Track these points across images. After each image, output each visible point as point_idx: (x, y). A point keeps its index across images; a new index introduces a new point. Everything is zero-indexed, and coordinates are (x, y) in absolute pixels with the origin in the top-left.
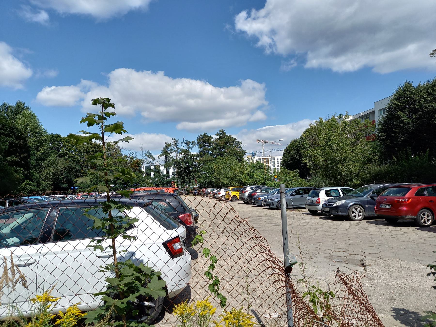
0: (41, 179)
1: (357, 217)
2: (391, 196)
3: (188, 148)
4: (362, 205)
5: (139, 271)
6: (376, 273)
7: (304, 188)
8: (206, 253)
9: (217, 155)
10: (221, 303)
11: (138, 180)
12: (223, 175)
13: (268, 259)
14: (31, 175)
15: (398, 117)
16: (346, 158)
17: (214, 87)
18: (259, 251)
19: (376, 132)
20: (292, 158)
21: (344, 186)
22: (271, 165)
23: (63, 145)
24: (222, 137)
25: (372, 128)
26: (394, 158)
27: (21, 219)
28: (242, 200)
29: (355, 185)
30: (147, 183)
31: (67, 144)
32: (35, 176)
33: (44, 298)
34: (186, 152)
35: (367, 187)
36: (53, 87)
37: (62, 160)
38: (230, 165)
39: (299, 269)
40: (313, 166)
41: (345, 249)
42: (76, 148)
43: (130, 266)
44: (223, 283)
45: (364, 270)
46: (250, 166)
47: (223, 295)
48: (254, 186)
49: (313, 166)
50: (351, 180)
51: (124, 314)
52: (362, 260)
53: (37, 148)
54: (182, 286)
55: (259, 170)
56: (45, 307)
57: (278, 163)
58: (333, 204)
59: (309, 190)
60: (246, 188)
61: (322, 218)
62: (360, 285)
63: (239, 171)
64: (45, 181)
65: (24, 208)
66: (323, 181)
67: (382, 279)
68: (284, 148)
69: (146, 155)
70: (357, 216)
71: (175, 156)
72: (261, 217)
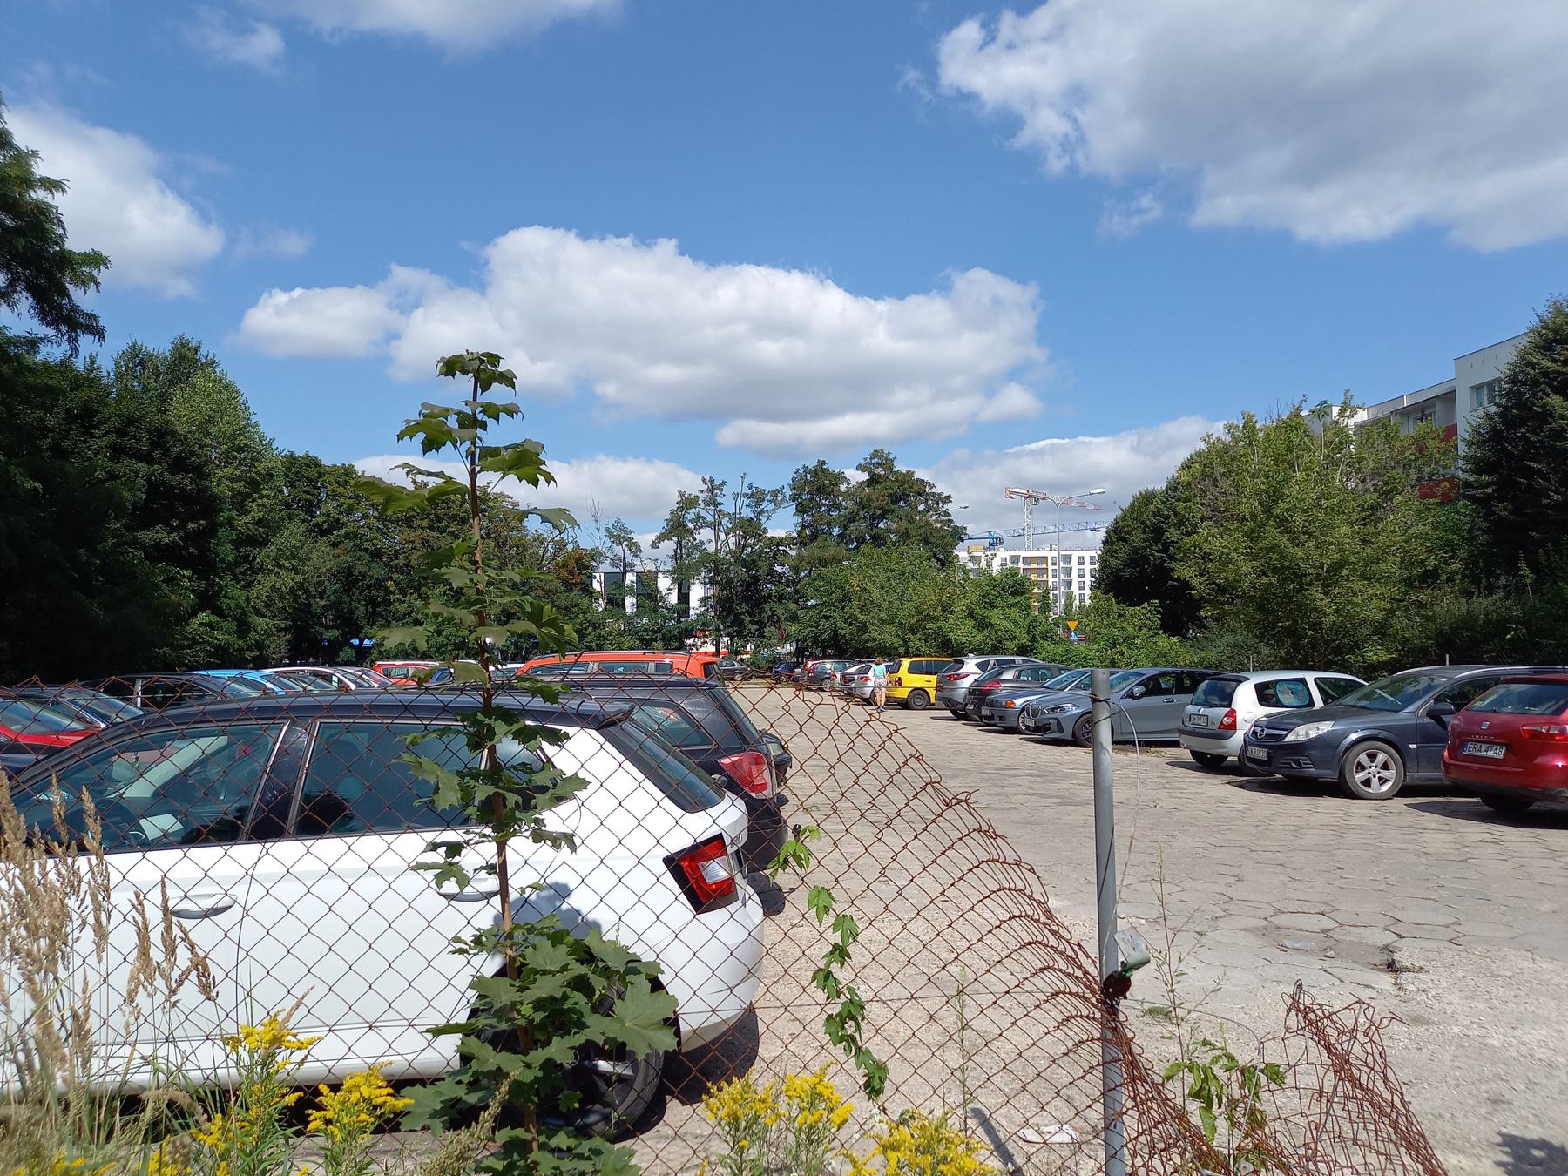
0: (253, 608)
1: (1375, 788)
2: (1507, 715)
3: (759, 515)
4: (1395, 741)
5: (586, 955)
6: (1438, 997)
7: (1178, 670)
8: (821, 905)
9: (861, 540)
10: (867, 1085)
11: (581, 624)
12: (882, 615)
13: (1051, 964)
14: (217, 594)
16: (1341, 564)
17: (852, 297)
18: (1008, 910)
19: (1460, 470)
20: (1136, 559)
21: (1325, 670)
22: (1057, 580)
23: (327, 495)
24: (879, 475)
25: (1444, 454)
26: (1525, 571)
27: (186, 754)
28: (947, 706)
29: (1371, 665)
30: (610, 633)
31: (341, 490)
32: (232, 598)
33: (268, 1037)
34: (750, 528)
35: (1415, 678)
36: (298, 292)
37: (323, 545)
38: (904, 578)
39: (1157, 974)
40: (1213, 590)
41: (1327, 904)
42: (372, 505)
43: (557, 938)
44: (874, 1011)
45: (1396, 984)
46: (977, 584)
47: (875, 1056)
48: (993, 659)
49: (1213, 590)
50: (1356, 647)
51: (533, 1102)
52: (1387, 949)
53: (240, 503)
54: (731, 1009)
55: (1013, 601)
56: (268, 1068)
57: (1081, 576)
58: (1285, 732)
59: (1196, 679)
60: (963, 663)
61: (1241, 786)
62: (1380, 1048)
63: (939, 600)
64: (264, 616)
65: (204, 717)
66: (1249, 647)
67: (1463, 1025)
68: (1106, 521)
69: (610, 535)
70: (1375, 781)
71: (710, 541)
72: (1014, 772)
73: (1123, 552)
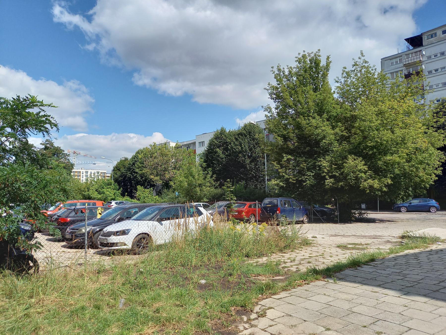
15: (216, 152)
50: (202, 199)
68: (115, 163)
73: (119, 173)
